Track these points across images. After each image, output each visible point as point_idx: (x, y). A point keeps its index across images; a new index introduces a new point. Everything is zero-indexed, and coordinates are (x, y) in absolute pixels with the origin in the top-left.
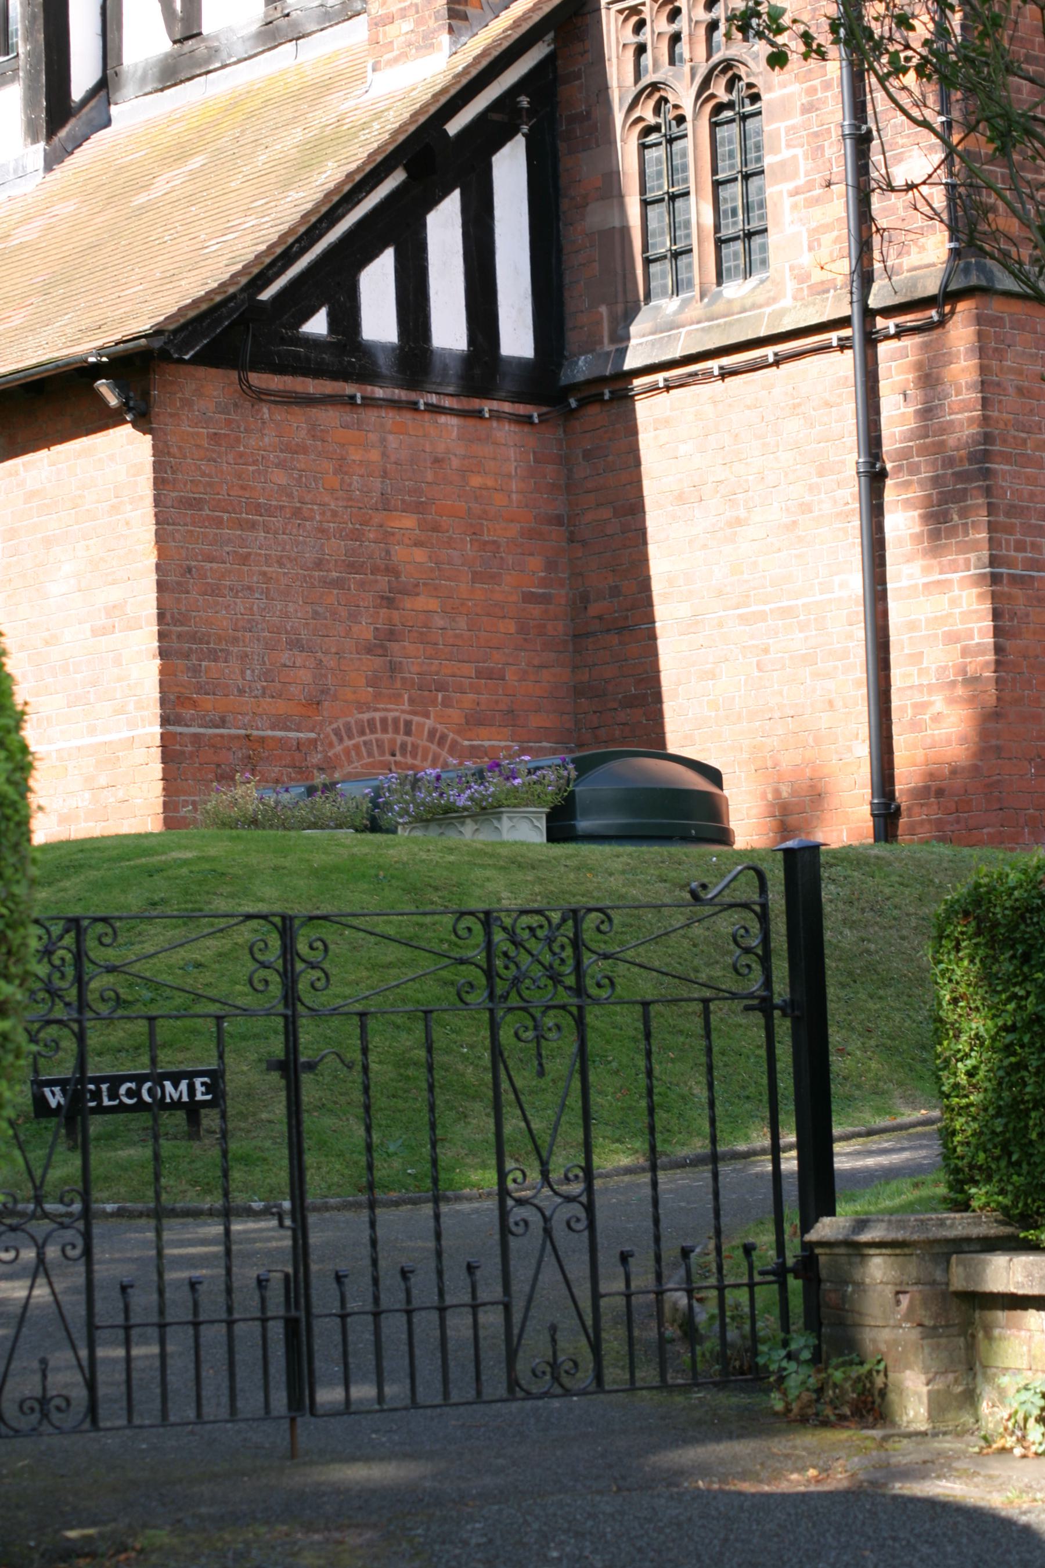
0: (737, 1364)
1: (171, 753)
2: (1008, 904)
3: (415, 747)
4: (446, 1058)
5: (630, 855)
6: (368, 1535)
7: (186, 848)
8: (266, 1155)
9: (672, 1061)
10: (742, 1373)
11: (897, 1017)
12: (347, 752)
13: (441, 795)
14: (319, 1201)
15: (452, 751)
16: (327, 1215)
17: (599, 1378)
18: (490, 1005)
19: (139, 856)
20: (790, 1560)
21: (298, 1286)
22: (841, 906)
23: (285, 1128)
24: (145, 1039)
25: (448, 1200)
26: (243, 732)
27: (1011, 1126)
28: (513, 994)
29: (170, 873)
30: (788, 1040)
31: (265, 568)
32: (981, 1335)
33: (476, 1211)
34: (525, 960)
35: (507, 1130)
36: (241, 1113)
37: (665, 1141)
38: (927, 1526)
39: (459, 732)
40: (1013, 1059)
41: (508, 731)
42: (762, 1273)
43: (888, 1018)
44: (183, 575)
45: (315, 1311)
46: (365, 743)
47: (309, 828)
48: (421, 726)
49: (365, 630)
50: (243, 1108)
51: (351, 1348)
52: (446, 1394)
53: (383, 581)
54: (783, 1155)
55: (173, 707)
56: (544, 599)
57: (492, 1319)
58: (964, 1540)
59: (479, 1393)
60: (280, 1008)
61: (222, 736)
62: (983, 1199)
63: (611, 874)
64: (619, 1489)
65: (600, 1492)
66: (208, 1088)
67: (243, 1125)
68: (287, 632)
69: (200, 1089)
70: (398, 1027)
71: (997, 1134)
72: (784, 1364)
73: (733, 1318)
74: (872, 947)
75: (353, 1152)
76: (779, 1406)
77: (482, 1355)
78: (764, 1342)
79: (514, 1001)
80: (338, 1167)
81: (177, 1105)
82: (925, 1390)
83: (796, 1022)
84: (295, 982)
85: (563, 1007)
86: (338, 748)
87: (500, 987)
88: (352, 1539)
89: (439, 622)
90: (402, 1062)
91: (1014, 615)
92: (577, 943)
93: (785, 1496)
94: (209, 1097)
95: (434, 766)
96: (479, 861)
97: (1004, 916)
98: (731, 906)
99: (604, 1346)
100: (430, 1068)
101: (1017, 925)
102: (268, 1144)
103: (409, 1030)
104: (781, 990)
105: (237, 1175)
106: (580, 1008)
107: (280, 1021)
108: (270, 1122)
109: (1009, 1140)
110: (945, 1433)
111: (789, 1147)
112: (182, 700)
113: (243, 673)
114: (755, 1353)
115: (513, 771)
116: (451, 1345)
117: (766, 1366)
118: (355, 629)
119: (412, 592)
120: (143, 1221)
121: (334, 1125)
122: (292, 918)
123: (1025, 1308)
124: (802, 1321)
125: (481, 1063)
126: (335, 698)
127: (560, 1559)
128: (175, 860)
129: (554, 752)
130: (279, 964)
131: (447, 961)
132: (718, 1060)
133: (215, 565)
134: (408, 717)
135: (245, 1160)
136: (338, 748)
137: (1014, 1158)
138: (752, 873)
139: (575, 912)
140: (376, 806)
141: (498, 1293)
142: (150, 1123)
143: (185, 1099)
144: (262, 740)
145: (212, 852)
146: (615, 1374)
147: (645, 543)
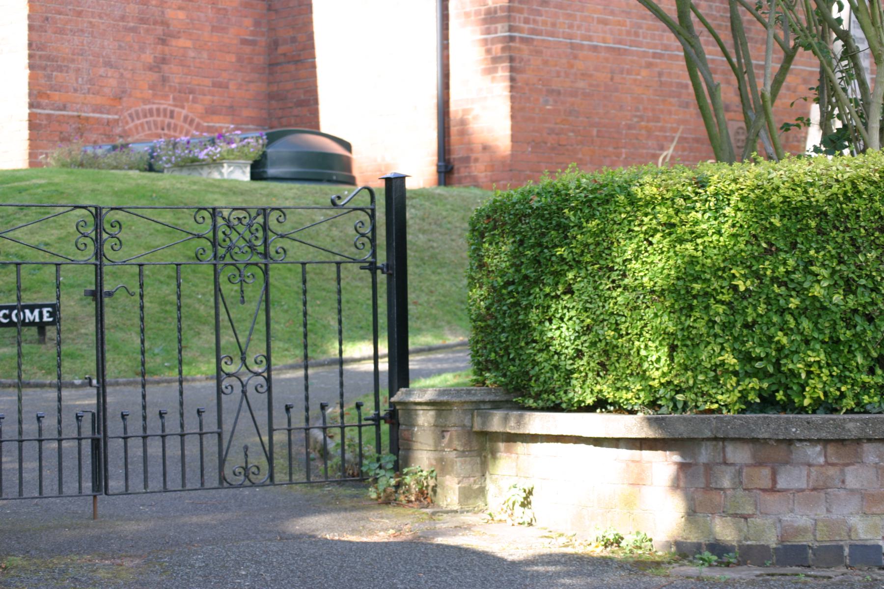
0: (351, 472)
1: (34, 125)
2: (512, 212)
3: (176, 126)
4: (188, 301)
5: (298, 189)
6: (137, 561)
7: (41, 177)
8: (83, 353)
9: (319, 306)
10: (353, 476)
11: (448, 285)
12: (136, 127)
13: (190, 152)
14: (113, 380)
15: (197, 129)
16: (118, 388)
17: (271, 477)
18: (214, 262)
19: (14, 182)
20: (377, 578)
21: (100, 416)
22: (418, 221)
23: (94, 338)
24: (15, 286)
25: (187, 380)
26: (75, 114)
27: (510, 338)
28: (228, 255)
29: (32, 191)
30: (385, 296)
31: (91, 20)
32: (489, 456)
33: (203, 387)
34: (234, 236)
35: (223, 342)
36: (69, 329)
37: (313, 351)
38: (456, 561)
39: (202, 118)
40: (512, 300)
41: (229, 118)
42: (367, 419)
43: (443, 285)
44: (43, 22)
45: (109, 434)
46: (147, 122)
47: (113, 169)
48: (180, 113)
49: (148, 57)
50: (70, 326)
51: (129, 460)
52: (184, 485)
53: (159, 29)
54: (380, 360)
55: (36, 99)
56: (253, 43)
57: (211, 443)
58: (477, 569)
59: (202, 484)
60: (93, 261)
61: (63, 116)
62: (493, 380)
63: (287, 199)
64: (281, 538)
65: (270, 540)
66: (51, 314)
67: (70, 336)
68: (103, 57)
69: (46, 315)
70: (161, 282)
71: (502, 343)
72: (378, 471)
73: (349, 446)
74: (435, 245)
75: (133, 353)
76: (374, 496)
77: (205, 465)
78: (366, 458)
79: (228, 260)
80: (125, 361)
81: (32, 323)
82: (457, 486)
83: (390, 277)
84: (102, 245)
85: (256, 264)
86: (131, 125)
87: (221, 251)
88: (127, 563)
89: (191, 54)
90: (163, 302)
91: (521, 60)
92: (265, 227)
93: (376, 544)
94: (51, 319)
95: (186, 136)
96: (211, 189)
97: (510, 219)
98: (355, 209)
99: (275, 461)
100: (179, 308)
101: (517, 224)
102: (85, 347)
103: (168, 284)
104: (382, 258)
105: (66, 364)
106: (266, 265)
107: (93, 268)
108: (86, 334)
109: (508, 346)
110: (468, 512)
111: (383, 356)
112: (41, 94)
113: (77, 79)
114: (361, 464)
115: (231, 139)
116: (187, 460)
117: (367, 473)
118: (143, 56)
119: (176, 36)
120: (11, 389)
121: (123, 338)
122: (101, 209)
123: (515, 442)
124: (388, 448)
125: (209, 304)
126: (130, 96)
127: (246, 575)
128: (35, 184)
129: (256, 130)
130: (93, 235)
131: (191, 236)
132: (344, 305)
133: (62, 17)
134: (172, 108)
135: (71, 356)
136: (131, 125)
137: (511, 356)
138: (366, 191)
139: (264, 210)
140: (152, 157)
141: (215, 428)
142: (16, 334)
143: (37, 320)
144: (87, 119)
145: (56, 180)
146: (279, 477)
147: (311, 12)
